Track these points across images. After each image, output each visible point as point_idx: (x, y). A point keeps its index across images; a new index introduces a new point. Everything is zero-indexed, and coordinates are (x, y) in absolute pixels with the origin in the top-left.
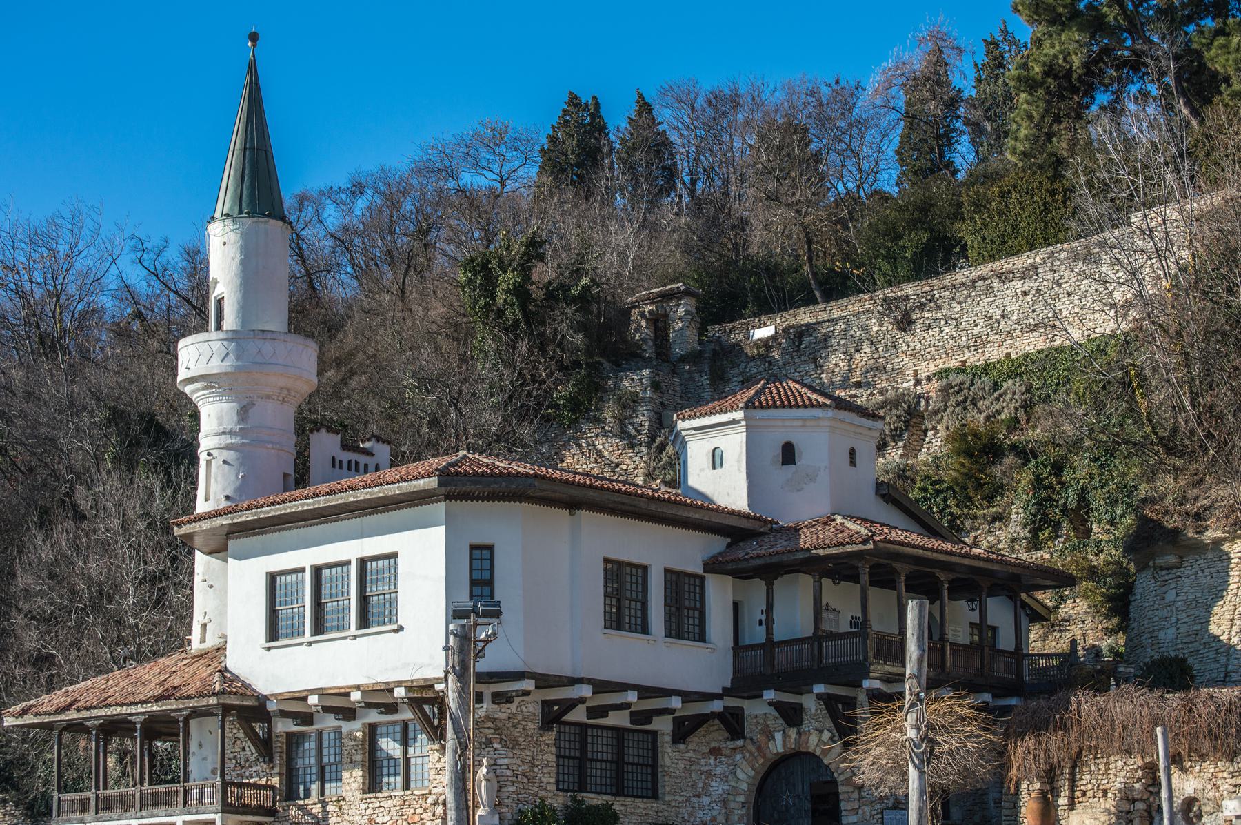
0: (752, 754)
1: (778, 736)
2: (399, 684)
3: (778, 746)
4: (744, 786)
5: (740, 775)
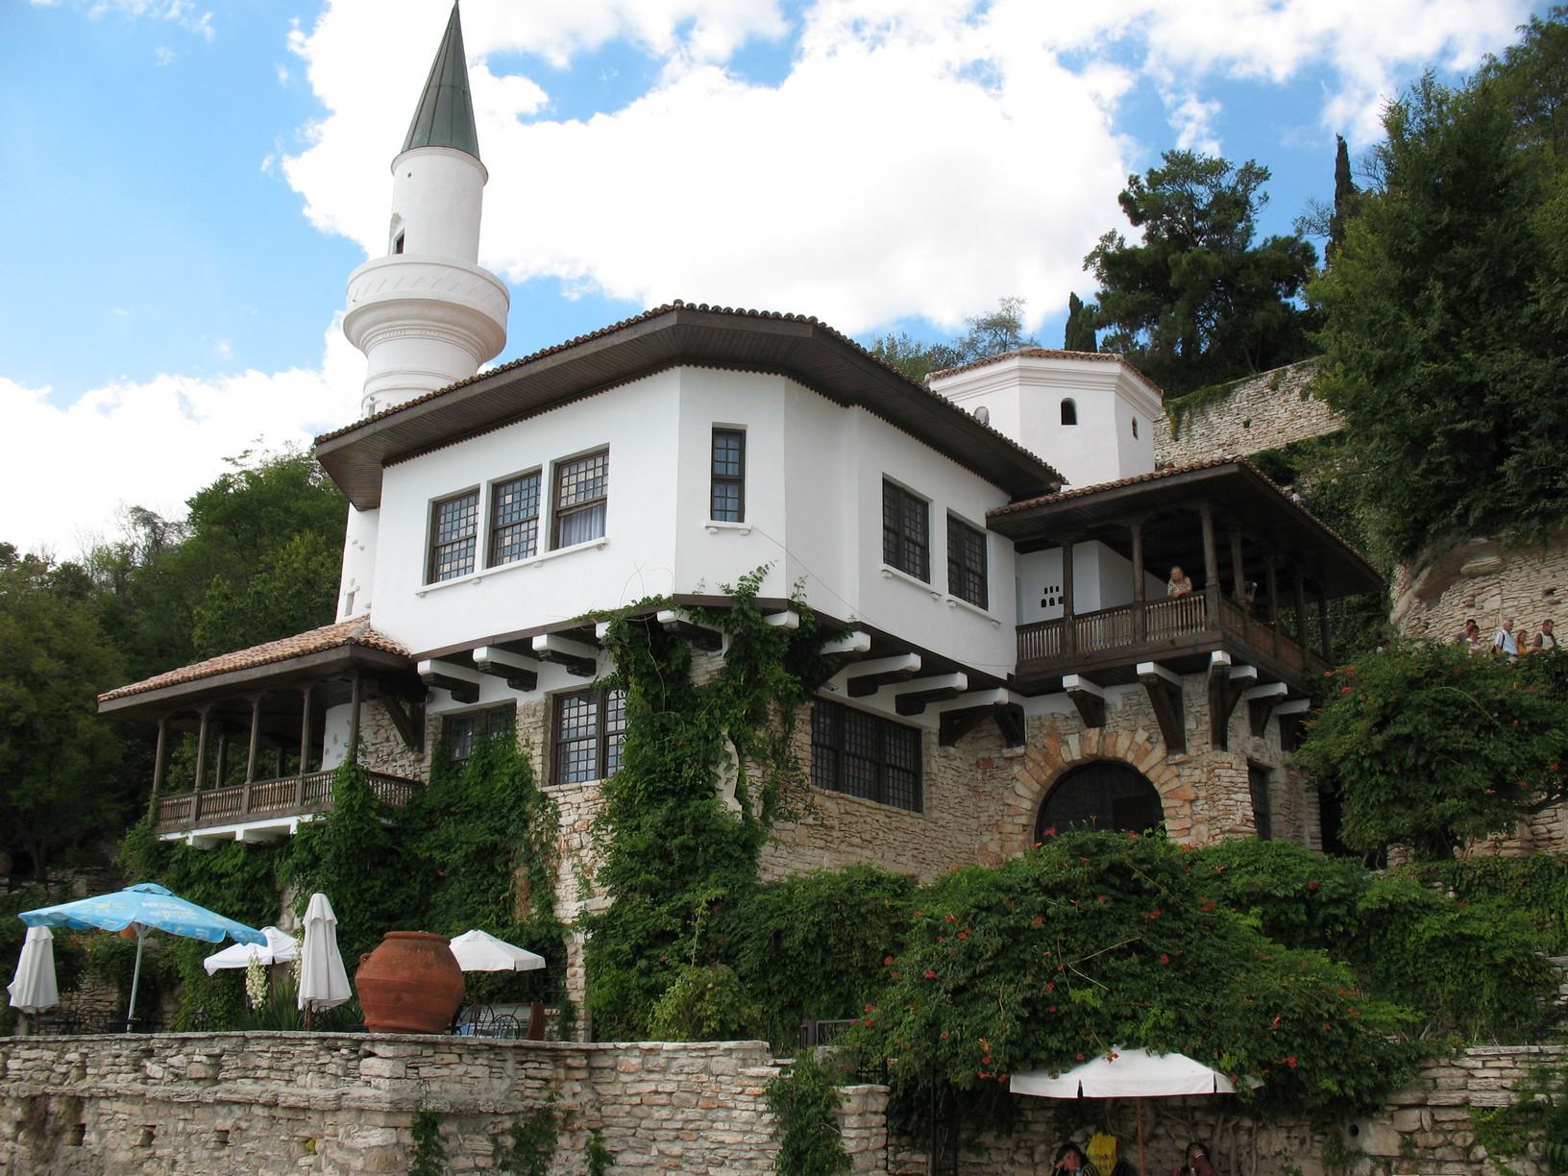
0: (1037, 763)
1: (1073, 741)
3: (1073, 750)
4: (1027, 805)
5: (1020, 789)
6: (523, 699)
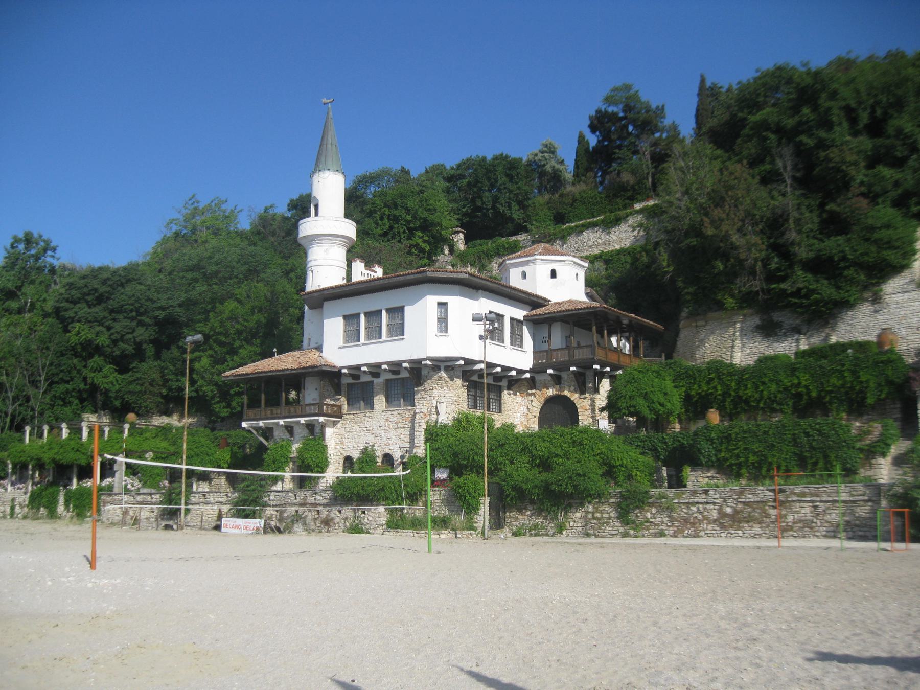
2: (405, 361)
6: (376, 381)
